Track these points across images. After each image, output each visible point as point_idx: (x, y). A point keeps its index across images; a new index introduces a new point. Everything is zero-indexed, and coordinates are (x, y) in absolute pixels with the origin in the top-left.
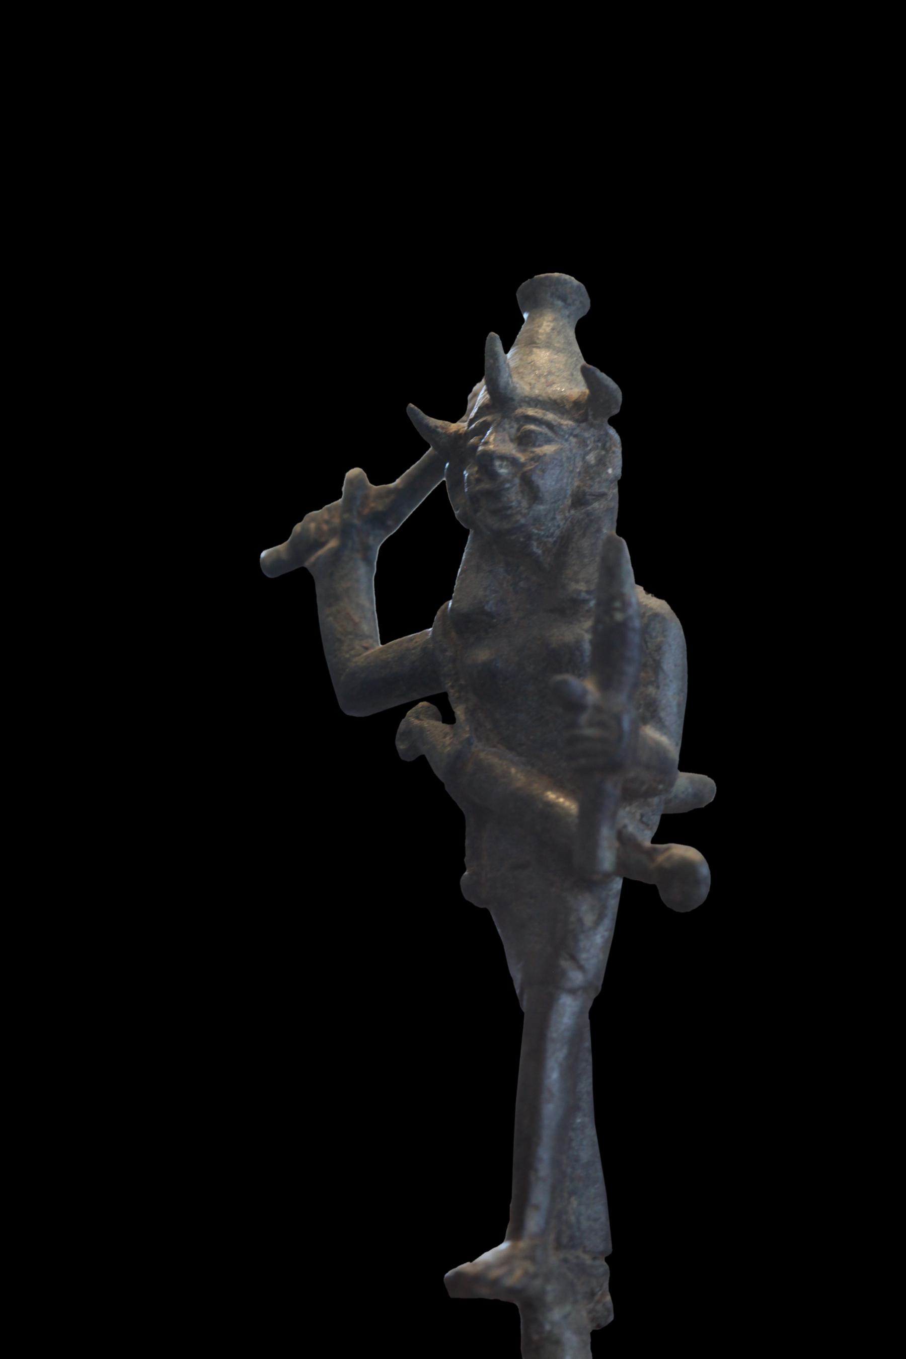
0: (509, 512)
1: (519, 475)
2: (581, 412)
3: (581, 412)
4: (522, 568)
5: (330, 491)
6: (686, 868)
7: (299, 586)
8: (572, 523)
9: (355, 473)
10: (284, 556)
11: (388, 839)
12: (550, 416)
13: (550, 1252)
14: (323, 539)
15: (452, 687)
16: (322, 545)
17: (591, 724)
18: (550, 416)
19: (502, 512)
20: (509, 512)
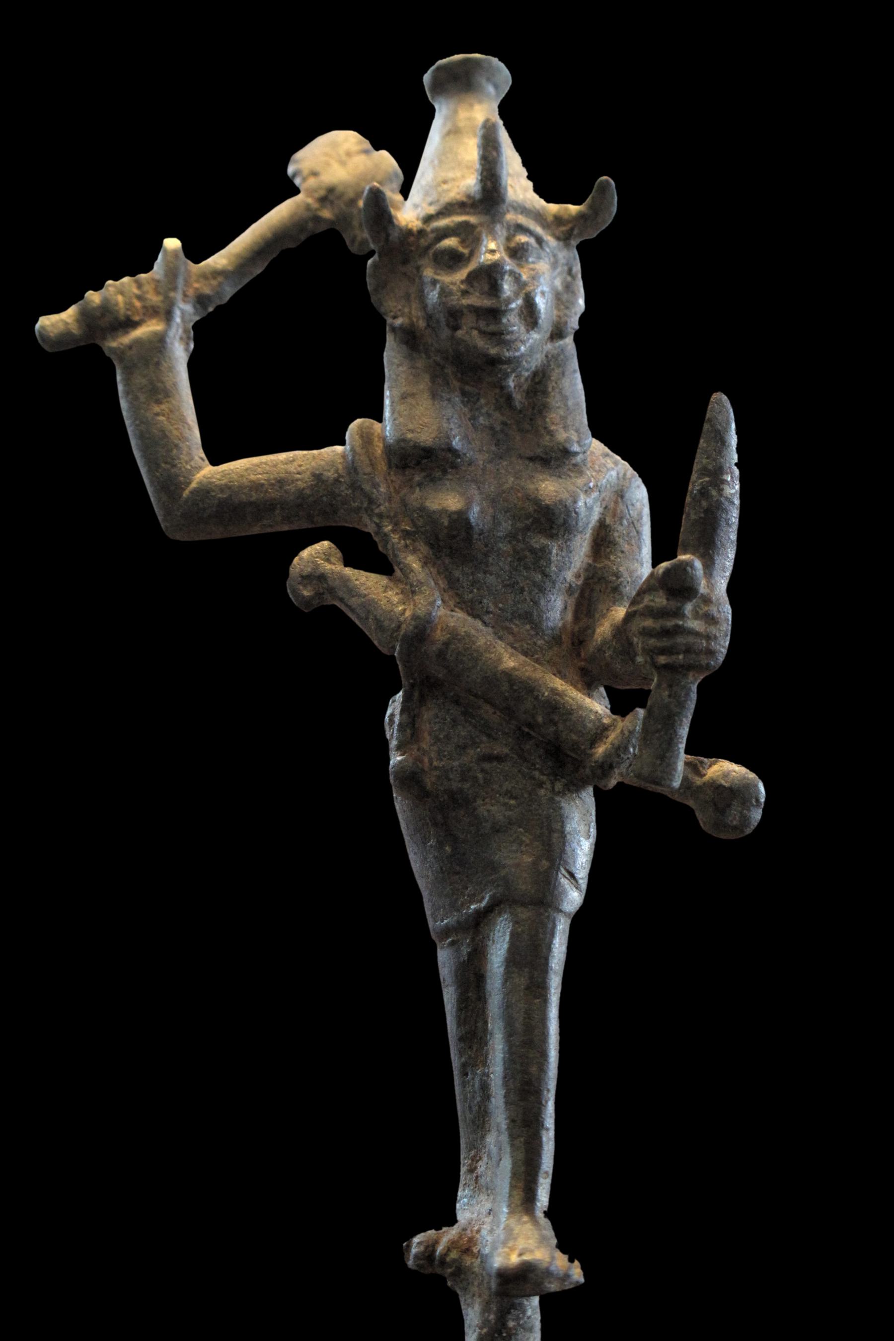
0: (508, 337)
1: (522, 295)
2: (564, 228)
3: (564, 228)
4: (482, 401)
5: (142, 262)
6: (728, 795)
7: (89, 367)
8: (547, 356)
9: (172, 244)
10: (75, 330)
11: (269, 699)
12: (539, 230)
13: (501, 1228)
14: (136, 318)
15: (393, 531)
16: (135, 325)
17: (696, 615)
18: (539, 230)
19: (498, 336)
20: (508, 337)
